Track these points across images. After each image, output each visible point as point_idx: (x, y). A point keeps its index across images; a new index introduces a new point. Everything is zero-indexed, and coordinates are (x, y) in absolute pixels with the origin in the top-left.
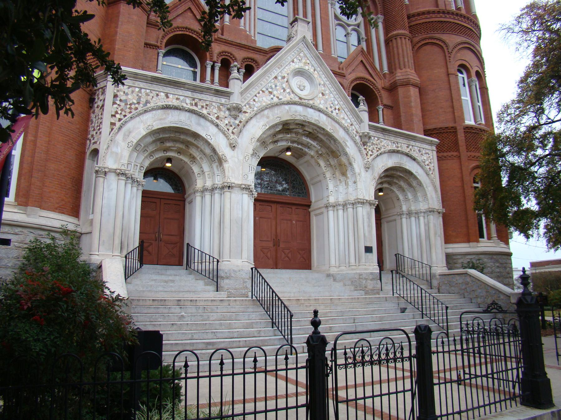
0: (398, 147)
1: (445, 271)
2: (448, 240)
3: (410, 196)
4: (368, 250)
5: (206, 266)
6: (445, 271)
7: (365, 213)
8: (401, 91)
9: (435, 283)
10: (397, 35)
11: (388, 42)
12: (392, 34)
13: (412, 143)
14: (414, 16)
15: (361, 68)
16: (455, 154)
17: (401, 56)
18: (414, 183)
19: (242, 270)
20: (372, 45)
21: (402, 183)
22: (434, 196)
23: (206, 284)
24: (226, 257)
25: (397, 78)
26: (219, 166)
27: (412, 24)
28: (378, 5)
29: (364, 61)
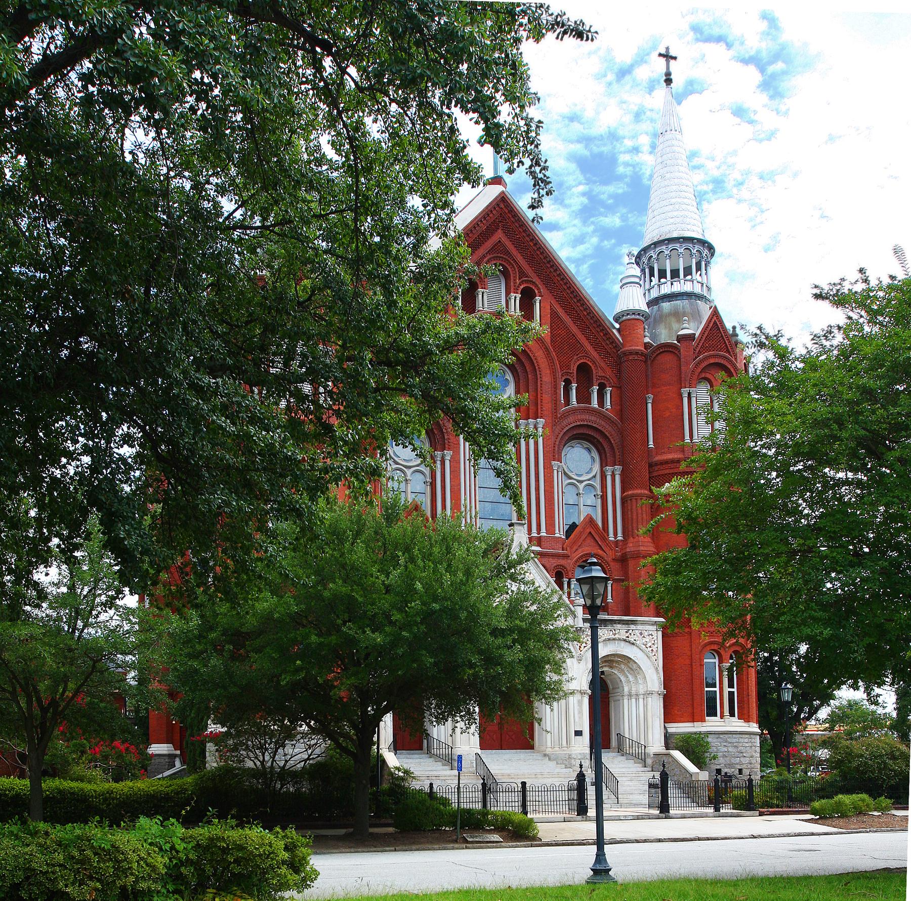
0: (615, 634)
1: (662, 750)
2: (669, 717)
3: (631, 678)
4: (578, 733)
5: (443, 751)
6: (662, 750)
7: (576, 702)
8: (631, 563)
9: (649, 761)
10: (632, 496)
11: (624, 501)
12: (630, 493)
13: (633, 627)
14: (656, 464)
15: (590, 541)
16: (687, 630)
17: (635, 521)
18: (635, 666)
19: (712, 255)
20: (424, 850)
21: (623, 666)
22: (655, 677)
23: (443, 765)
24: (458, 745)
25: (628, 550)
26: (579, 149)
27: (655, 474)
28: (616, 451)
29: (593, 533)
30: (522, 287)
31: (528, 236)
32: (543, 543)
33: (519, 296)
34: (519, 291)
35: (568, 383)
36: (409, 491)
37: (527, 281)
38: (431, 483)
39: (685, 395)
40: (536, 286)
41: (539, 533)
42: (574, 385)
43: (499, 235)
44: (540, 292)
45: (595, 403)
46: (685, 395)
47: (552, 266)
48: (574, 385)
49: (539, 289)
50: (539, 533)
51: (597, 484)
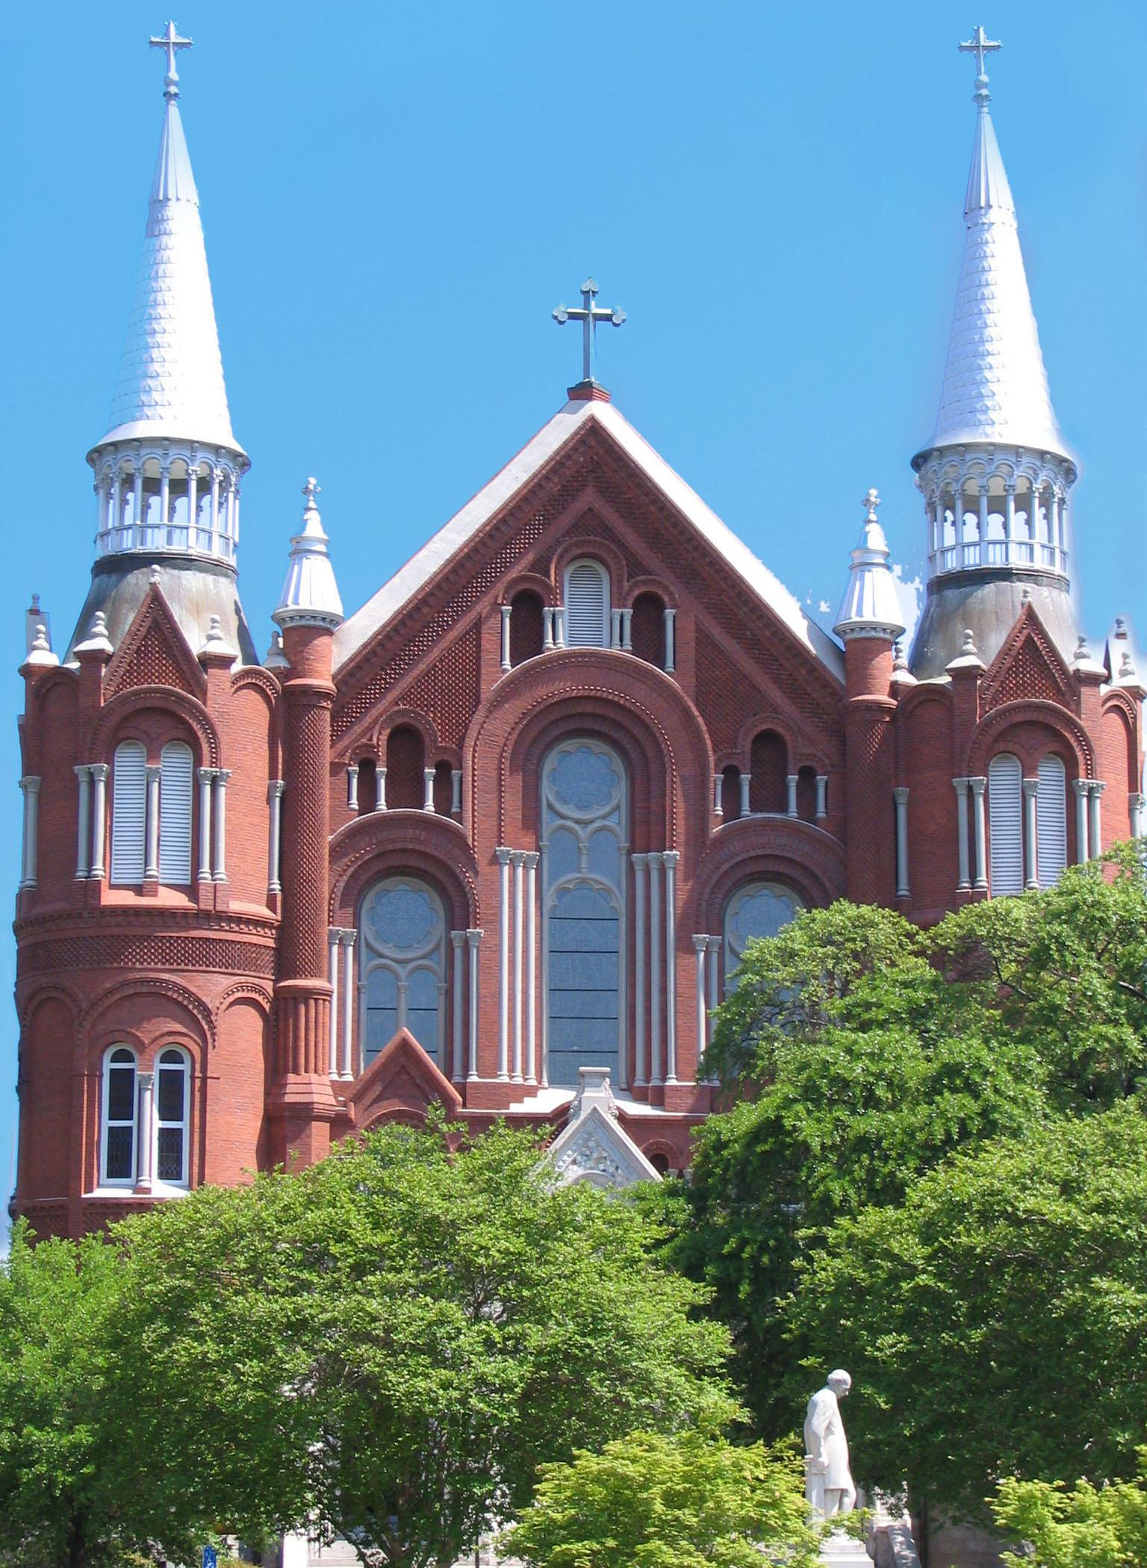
30: (636, 593)
31: (647, 494)
32: (667, 1101)
33: (628, 612)
34: (630, 601)
35: (731, 774)
36: (403, 1007)
37: (645, 583)
38: (447, 991)
39: (83, 779)
40: (666, 588)
41: (648, 1080)
42: (746, 778)
43: (589, 498)
44: (673, 599)
45: (430, 807)
46: (83, 779)
47: (696, 548)
48: (746, 778)
49: (670, 594)
50: (648, 1080)
51: (438, 966)
